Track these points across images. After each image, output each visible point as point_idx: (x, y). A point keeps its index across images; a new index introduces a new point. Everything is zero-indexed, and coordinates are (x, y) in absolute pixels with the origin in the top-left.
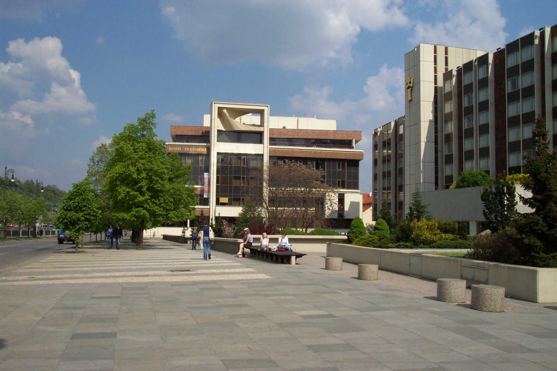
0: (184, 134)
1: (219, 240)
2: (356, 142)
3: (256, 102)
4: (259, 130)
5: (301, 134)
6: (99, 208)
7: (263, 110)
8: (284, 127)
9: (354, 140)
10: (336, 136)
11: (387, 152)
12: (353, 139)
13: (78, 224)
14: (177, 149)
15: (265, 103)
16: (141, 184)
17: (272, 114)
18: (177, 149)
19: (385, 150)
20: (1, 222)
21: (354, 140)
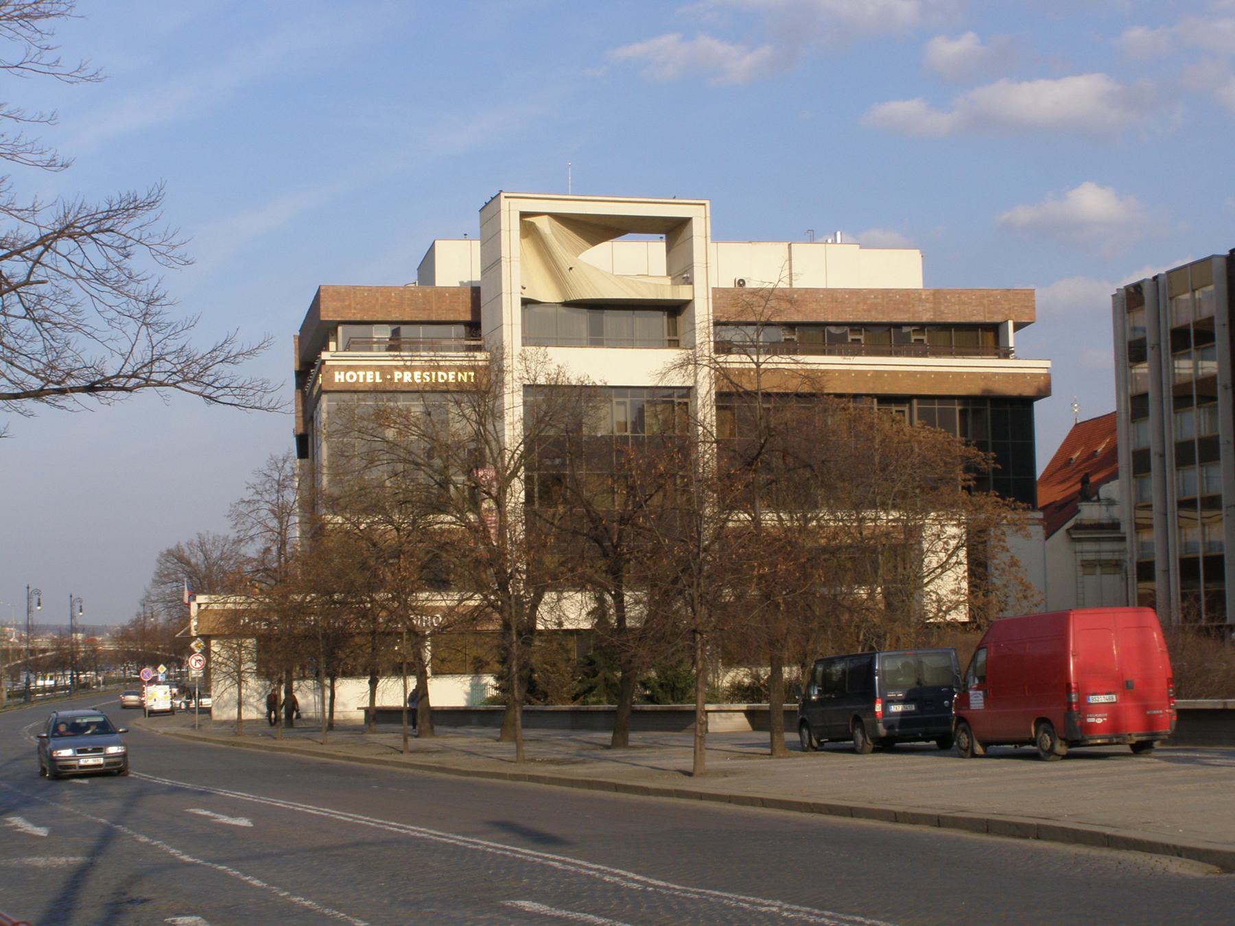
0: (822, 320)
1: (681, 709)
2: (1018, 327)
3: (674, 196)
4: (676, 298)
5: (814, 305)
6: (405, 584)
7: (683, 223)
8: (741, 283)
9: (1011, 324)
10: (942, 313)
11: (456, 378)
12: (1007, 321)
13: (407, 640)
14: (365, 377)
15: (694, 194)
16: (536, 503)
17: (720, 234)
18: (365, 377)
19: (1212, 359)
20: (1232, 628)
21: (1011, 324)
